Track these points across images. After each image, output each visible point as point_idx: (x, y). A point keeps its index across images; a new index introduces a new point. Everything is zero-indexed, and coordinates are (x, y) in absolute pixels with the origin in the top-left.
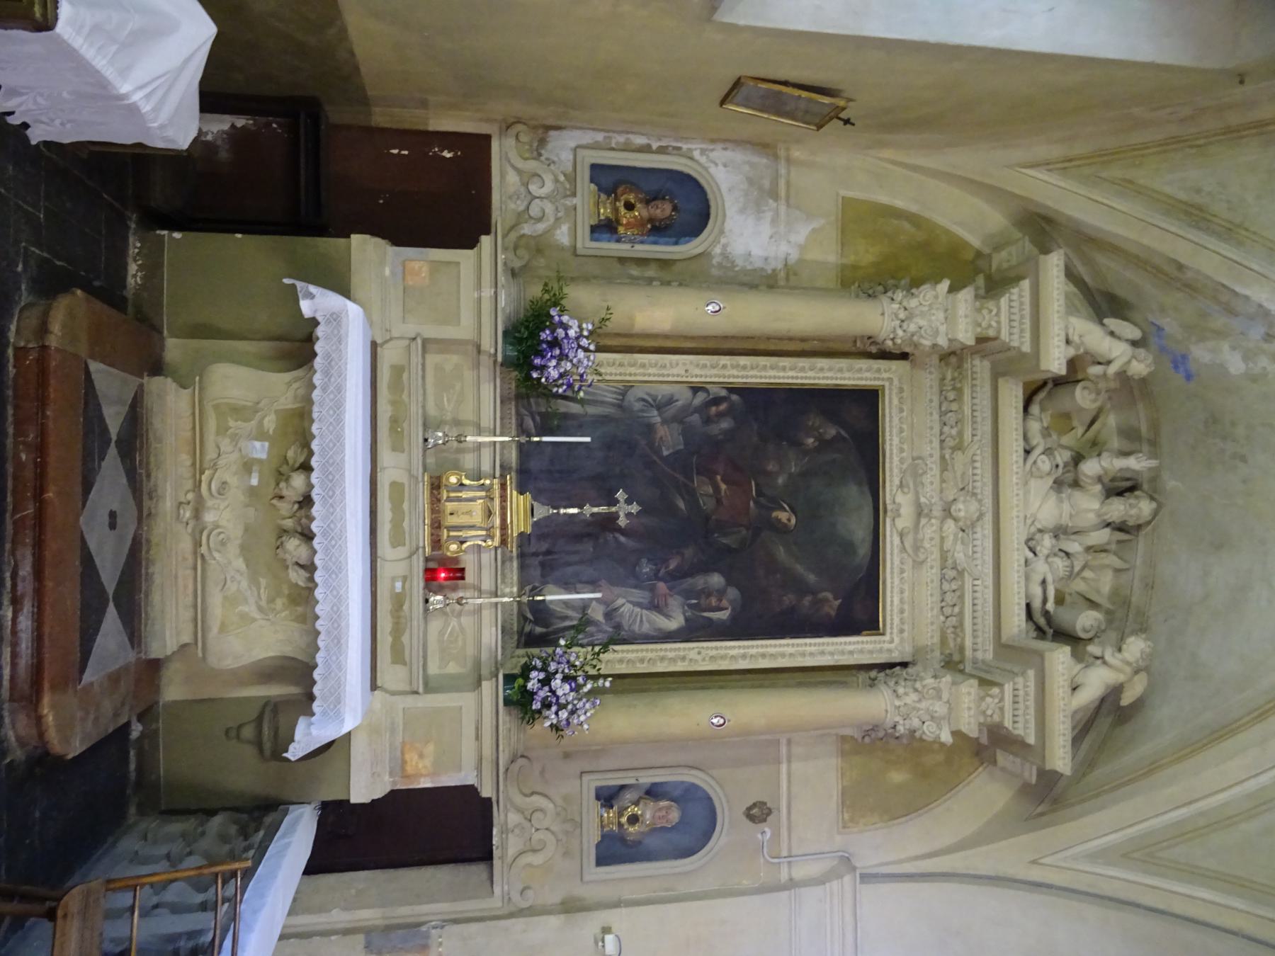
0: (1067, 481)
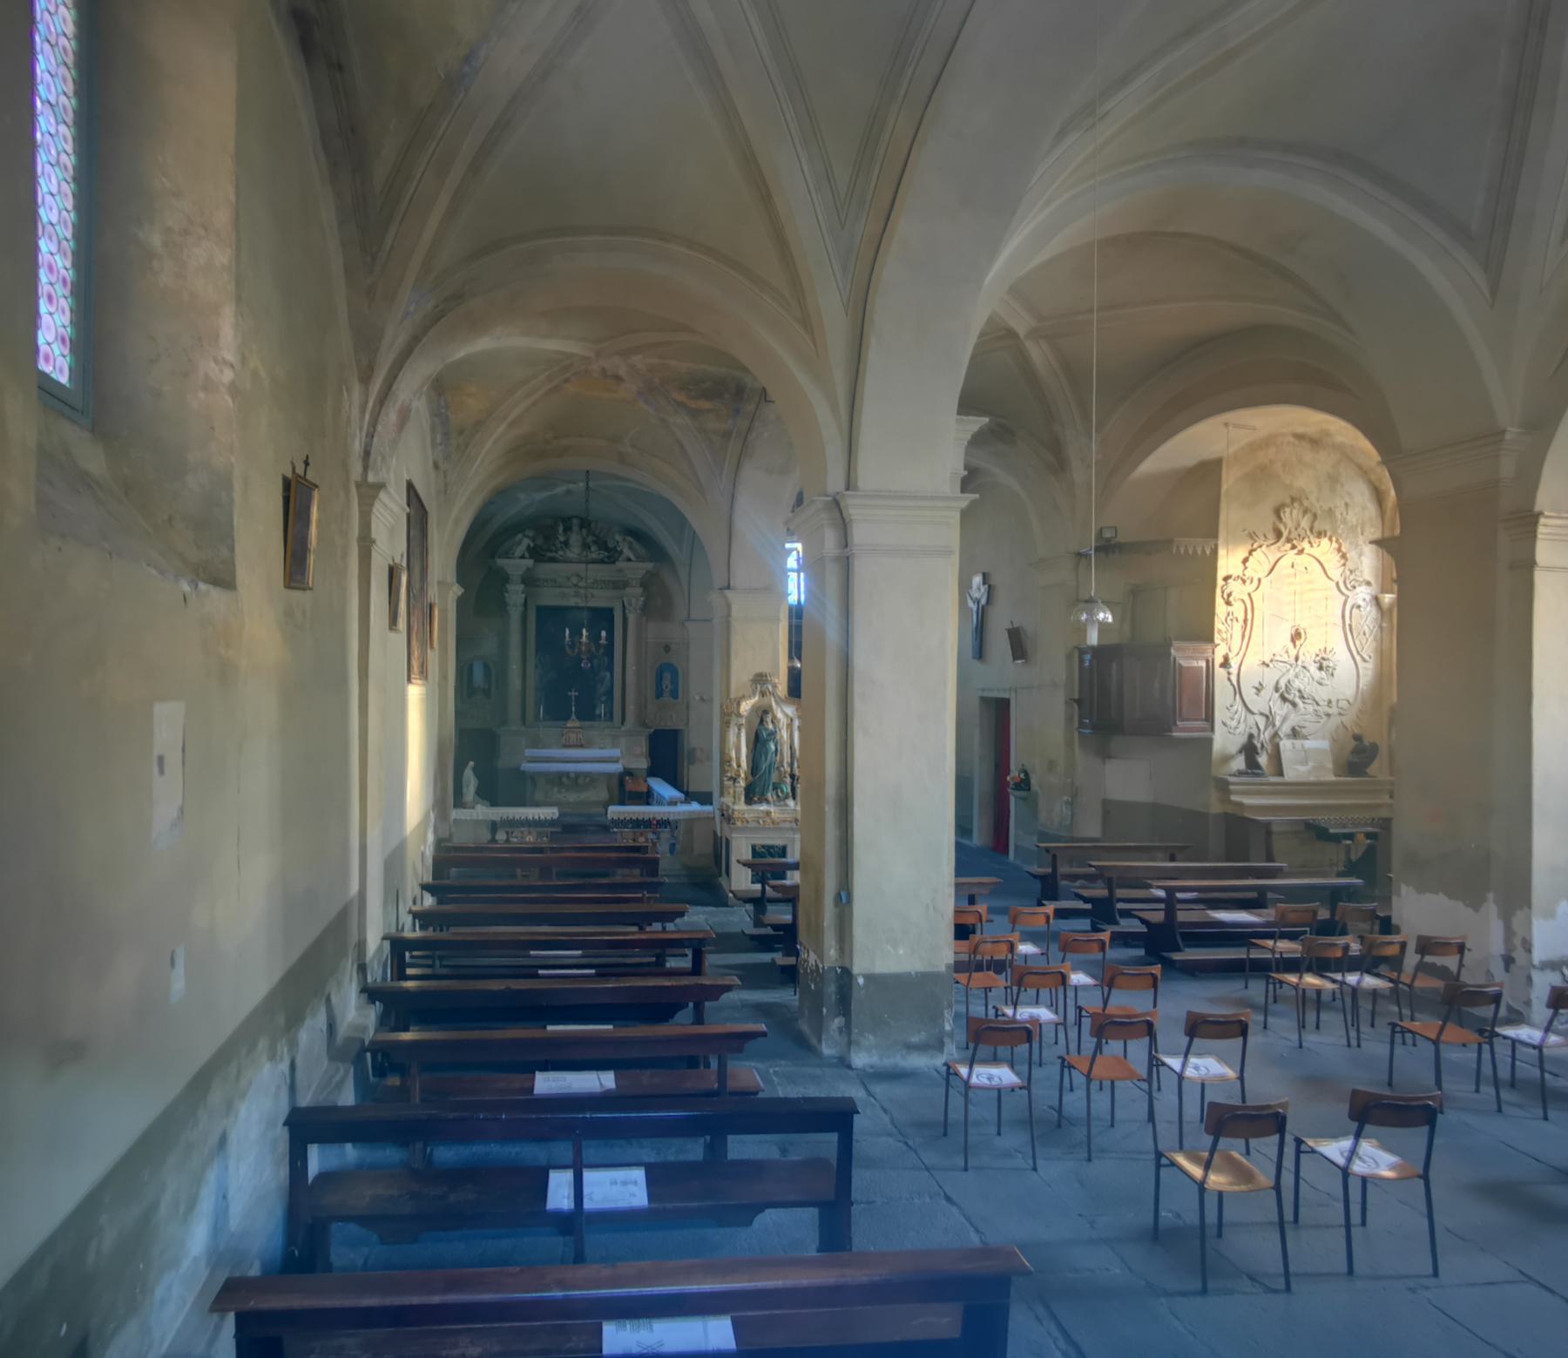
0: (566, 543)
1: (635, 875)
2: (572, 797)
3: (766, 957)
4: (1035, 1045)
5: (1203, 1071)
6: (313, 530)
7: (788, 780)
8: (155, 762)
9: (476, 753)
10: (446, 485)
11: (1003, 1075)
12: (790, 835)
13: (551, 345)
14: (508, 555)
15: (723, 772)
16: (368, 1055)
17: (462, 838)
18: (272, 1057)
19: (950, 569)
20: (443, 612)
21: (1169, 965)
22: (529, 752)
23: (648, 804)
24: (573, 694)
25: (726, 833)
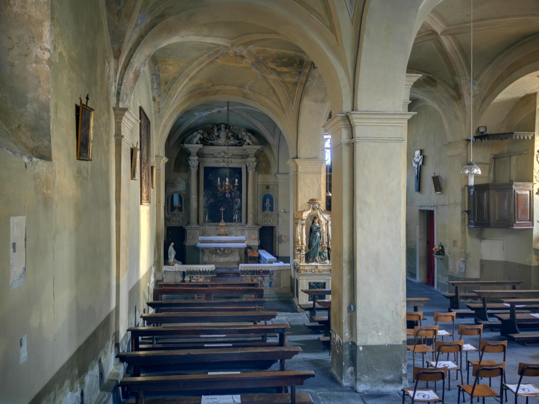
0: (218, 137)
1: (252, 297)
2: (222, 260)
3: (315, 337)
4: (446, 380)
5: (526, 391)
6: (91, 132)
7: (326, 251)
8: (11, 247)
9: (174, 240)
10: (159, 109)
11: (431, 395)
12: (327, 277)
13: (209, 40)
14: (190, 142)
15: (295, 247)
16: (120, 388)
17: (169, 279)
18: (72, 389)
19: (402, 150)
20: (158, 170)
21: (511, 340)
22: (201, 238)
23: (259, 263)
24: (222, 209)
25: (297, 276)
